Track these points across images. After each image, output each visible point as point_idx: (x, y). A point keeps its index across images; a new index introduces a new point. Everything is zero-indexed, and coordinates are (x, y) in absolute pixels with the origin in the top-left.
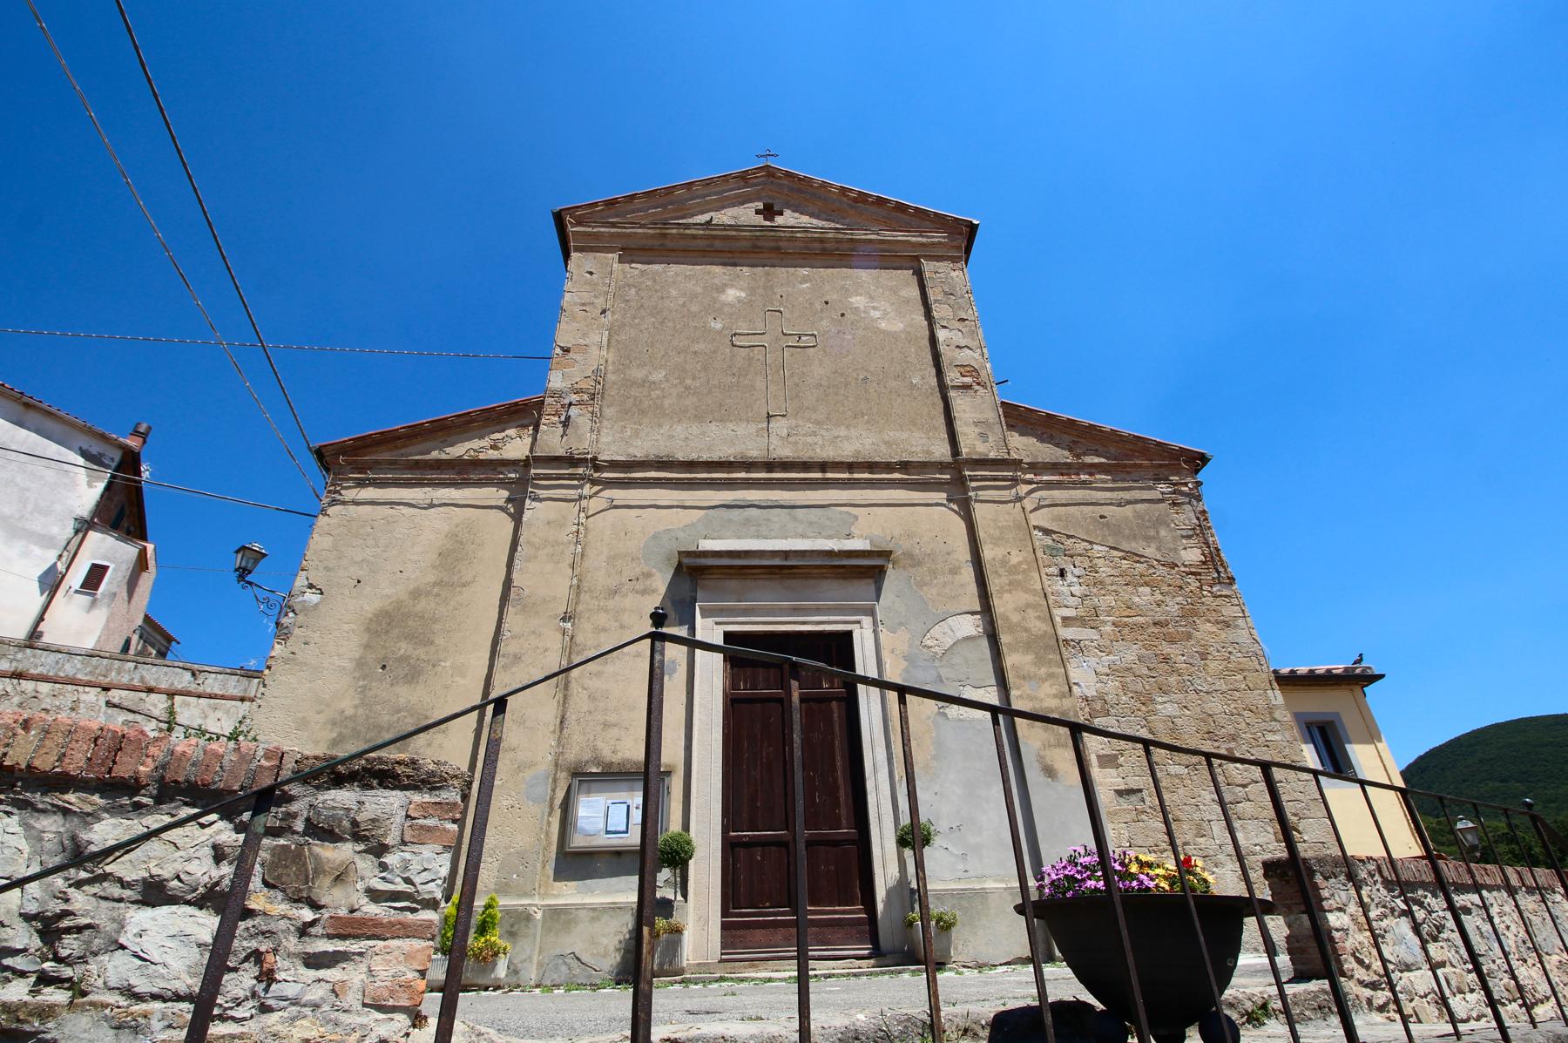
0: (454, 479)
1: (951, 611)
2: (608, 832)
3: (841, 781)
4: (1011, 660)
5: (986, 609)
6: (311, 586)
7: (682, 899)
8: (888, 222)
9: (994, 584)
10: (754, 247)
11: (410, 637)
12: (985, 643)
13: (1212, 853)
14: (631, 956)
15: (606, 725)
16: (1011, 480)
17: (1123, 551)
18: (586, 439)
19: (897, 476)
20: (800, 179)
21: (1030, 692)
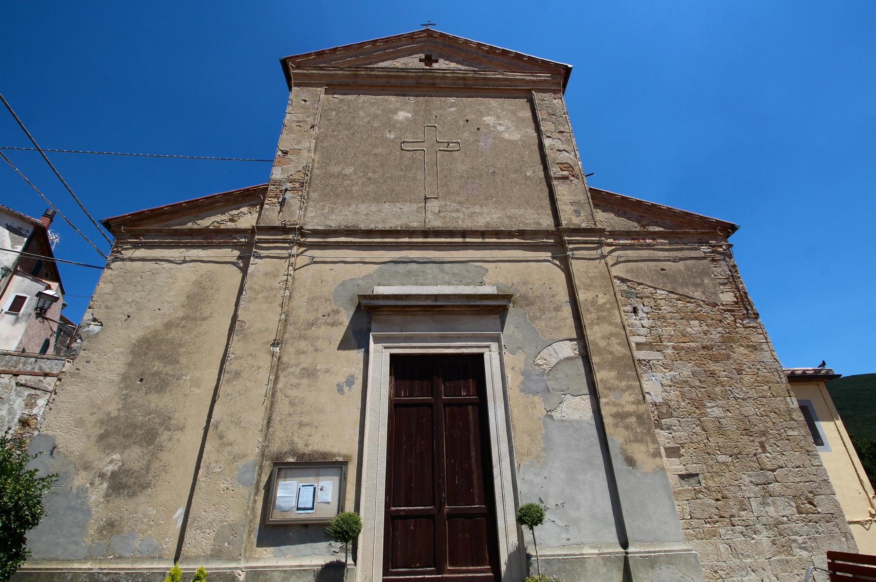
0: (202, 242)
3: (474, 467)
4: (600, 375)
5: (581, 337)
8: (510, 66)
10: (418, 83)
11: (162, 358)
12: (580, 362)
15: (301, 425)
16: (597, 243)
19: (516, 240)
20: (450, 38)
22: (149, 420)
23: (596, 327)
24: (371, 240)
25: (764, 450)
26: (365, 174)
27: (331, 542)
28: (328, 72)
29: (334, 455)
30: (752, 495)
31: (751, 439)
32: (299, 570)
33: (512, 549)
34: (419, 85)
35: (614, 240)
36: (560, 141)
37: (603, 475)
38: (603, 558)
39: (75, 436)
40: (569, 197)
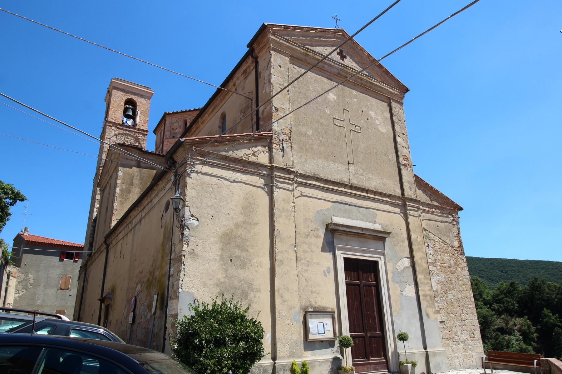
0: (242, 169)
1: (402, 256)
2: (319, 334)
3: (376, 316)
4: (419, 277)
5: (412, 257)
6: (192, 216)
7: (342, 357)
8: (382, 77)
9: (415, 248)
10: (339, 73)
11: (239, 247)
12: (411, 269)
13: (458, 341)
14: (76, 331)
15: (312, 292)
16: (418, 208)
17: (442, 240)
18: (291, 161)
19: (387, 199)
20: (354, 42)
21: (423, 288)
22: (242, 285)
23: (417, 253)
24: (328, 186)
25: (463, 313)
26: (319, 138)
27: (332, 348)
28: (292, 46)
29: (327, 308)
30: (459, 330)
31: (460, 308)
32: (325, 361)
33: (393, 350)
34: (340, 76)
35: (422, 207)
36: (403, 140)
37: (418, 321)
38: (420, 354)
39: (204, 293)
40: (407, 178)
